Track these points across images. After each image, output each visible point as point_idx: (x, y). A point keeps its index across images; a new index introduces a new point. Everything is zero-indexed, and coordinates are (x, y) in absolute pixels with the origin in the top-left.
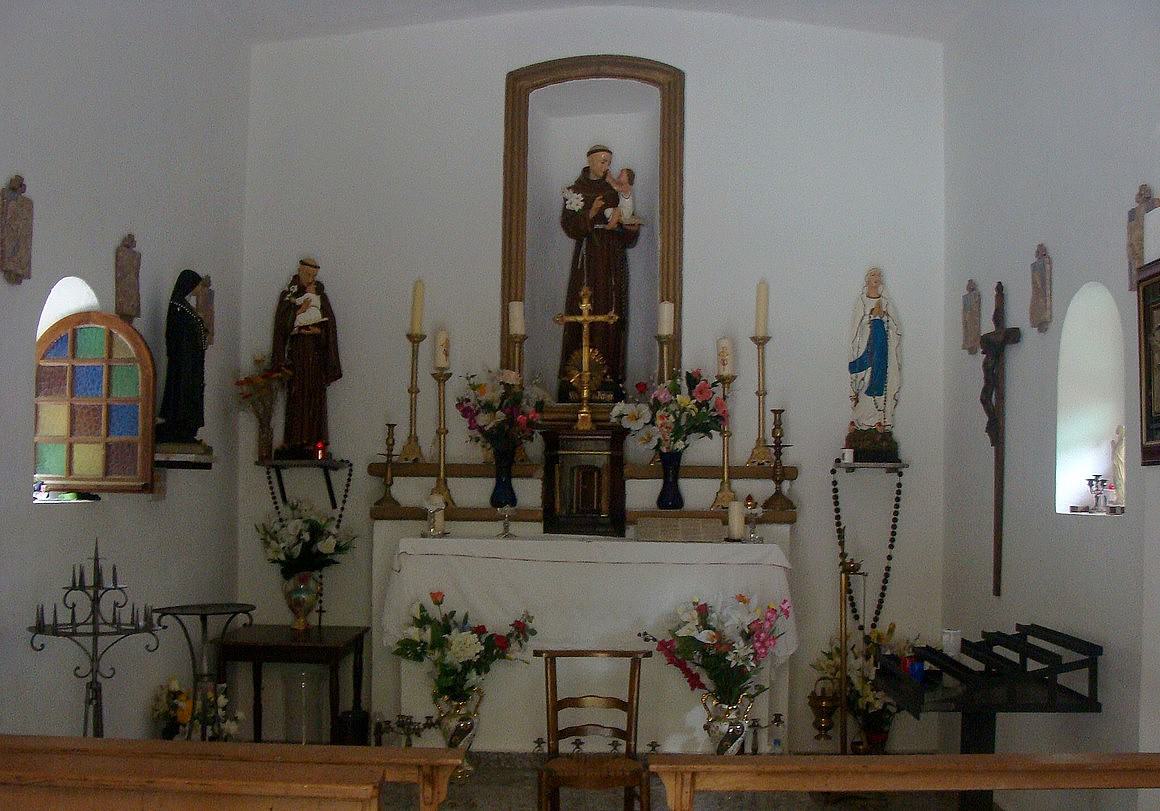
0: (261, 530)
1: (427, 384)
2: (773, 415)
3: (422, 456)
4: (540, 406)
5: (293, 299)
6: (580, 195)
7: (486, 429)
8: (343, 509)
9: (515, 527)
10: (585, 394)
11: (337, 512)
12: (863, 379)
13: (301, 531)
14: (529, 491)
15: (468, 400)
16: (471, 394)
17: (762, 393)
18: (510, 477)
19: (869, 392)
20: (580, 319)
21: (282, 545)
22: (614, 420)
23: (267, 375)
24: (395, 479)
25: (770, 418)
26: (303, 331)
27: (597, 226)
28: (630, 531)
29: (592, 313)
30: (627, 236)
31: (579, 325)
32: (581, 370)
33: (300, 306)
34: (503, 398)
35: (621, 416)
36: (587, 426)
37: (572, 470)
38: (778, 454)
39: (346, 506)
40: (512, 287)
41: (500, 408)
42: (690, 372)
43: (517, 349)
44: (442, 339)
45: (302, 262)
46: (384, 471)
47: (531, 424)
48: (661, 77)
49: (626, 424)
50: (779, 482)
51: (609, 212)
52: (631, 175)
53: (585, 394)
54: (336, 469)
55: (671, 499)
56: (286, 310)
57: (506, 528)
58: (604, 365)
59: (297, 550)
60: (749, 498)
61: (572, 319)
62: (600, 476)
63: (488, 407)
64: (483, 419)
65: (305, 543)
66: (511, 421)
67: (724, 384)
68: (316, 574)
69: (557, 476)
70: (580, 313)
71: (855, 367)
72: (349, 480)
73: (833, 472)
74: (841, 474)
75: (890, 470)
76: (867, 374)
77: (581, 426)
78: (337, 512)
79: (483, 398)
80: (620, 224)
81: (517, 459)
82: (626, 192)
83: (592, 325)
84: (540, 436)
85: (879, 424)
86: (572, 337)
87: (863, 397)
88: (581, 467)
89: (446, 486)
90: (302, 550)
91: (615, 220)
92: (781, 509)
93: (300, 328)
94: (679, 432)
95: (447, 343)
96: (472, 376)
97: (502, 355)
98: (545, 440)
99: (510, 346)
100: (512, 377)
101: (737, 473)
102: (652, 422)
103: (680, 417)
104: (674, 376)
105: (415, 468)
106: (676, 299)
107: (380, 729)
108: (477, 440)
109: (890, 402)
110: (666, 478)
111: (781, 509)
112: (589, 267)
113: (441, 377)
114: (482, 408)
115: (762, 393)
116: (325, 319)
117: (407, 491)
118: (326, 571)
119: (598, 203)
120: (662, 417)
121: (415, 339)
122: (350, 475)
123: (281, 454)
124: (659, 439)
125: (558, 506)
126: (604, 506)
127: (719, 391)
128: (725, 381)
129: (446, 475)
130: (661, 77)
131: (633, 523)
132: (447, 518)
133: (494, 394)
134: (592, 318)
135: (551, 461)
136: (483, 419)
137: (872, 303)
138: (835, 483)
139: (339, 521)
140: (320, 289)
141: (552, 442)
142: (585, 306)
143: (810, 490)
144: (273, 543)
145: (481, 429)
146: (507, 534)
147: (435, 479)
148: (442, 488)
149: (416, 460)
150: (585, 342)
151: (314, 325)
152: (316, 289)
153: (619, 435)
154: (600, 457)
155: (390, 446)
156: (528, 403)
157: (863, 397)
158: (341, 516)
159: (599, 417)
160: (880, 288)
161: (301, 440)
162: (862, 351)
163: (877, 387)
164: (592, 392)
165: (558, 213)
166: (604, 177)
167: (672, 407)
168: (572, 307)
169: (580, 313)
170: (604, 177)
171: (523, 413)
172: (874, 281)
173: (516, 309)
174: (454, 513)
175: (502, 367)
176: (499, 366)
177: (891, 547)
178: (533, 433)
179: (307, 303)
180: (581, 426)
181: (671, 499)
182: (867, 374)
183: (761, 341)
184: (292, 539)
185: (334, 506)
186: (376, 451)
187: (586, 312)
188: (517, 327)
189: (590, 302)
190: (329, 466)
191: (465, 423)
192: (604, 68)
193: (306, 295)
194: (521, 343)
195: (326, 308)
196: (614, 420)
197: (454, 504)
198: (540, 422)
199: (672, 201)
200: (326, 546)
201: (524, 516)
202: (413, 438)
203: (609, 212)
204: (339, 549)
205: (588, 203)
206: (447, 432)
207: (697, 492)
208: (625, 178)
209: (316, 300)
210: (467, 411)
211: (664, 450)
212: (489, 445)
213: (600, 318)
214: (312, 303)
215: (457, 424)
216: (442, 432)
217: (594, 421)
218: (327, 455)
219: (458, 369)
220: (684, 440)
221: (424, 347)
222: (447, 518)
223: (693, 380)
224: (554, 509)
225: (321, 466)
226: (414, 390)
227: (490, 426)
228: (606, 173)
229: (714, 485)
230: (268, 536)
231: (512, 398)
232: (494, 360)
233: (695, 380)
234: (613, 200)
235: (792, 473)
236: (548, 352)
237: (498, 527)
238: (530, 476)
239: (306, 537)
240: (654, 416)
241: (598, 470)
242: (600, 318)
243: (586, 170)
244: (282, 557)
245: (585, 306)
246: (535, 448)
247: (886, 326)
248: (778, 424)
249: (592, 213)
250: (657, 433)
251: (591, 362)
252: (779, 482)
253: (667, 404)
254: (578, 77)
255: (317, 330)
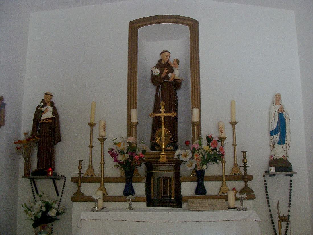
0: (24, 206)
1: (97, 144)
2: (243, 153)
3: (94, 174)
4: (144, 152)
5: (41, 109)
6: (158, 69)
7: (121, 161)
8: (61, 196)
9: (135, 205)
10: (163, 146)
11: (59, 197)
12: (276, 138)
13: (41, 206)
14: (140, 188)
15: (113, 150)
16: (115, 147)
17: (235, 145)
18: (131, 182)
19: (279, 143)
20: (160, 115)
21: (33, 213)
22: (176, 157)
23: (28, 140)
24: (83, 184)
25: (240, 155)
26: (44, 121)
27: (165, 81)
28: (184, 205)
29: (165, 112)
30: (177, 84)
31: (160, 118)
32: (160, 137)
33: (43, 112)
34: (128, 149)
35: (179, 155)
36: (165, 160)
37: (158, 179)
38: (245, 170)
39: (63, 195)
40: (132, 103)
41: (127, 152)
42: (208, 136)
43: (134, 128)
44: (102, 124)
45: (45, 94)
46: (78, 180)
47: (140, 159)
48: (189, 23)
49: (181, 158)
50: (246, 182)
51: (170, 75)
52: (178, 61)
53: (163, 146)
54: (59, 179)
55: (200, 191)
56: (39, 112)
57: (130, 205)
58: (170, 134)
59: (40, 215)
60: (234, 189)
61: (157, 115)
62: (170, 182)
63: (122, 152)
64: (120, 158)
65: (43, 212)
66: (132, 158)
67: (222, 141)
68: (50, 225)
69: (152, 182)
70: (160, 112)
71: (272, 133)
72: (64, 184)
73: (264, 176)
74: (268, 178)
75: (287, 175)
76: (278, 136)
77: (161, 160)
78: (59, 197)
79: (120, 148)
80: (174, 80)
81: (135, 175)
82: (176, 67)
83: (165, 117)
84: (144, 165)
85: (284, 156)
86: (157, 123)
87: (276, 145)
88: (162, 178)
89: (104, 187)
90: (42, 214)
91: (173, 78)
92: (250, 195)
93: (43, 120)
94: (205, 161)
95: (105, 125)
96: (115, 139)
97: (128, 132)
98: (146, 166)
99: (131, 127)
100: (132, 140)
101: (228, 178)
102: (193, 158)
103: (205, 155)
104: (200, 138)
105: (91, 179)
106: (199, 107)
107: (98, 190)
108: (117, 166)
109: (288, 147)
110: (198, 182)
111: (250, 195)
112: (162, 96)
113: (102, 139)
114: (119, 153)
115: (235, 145)
116: (54, 116)
117: (88, 189)
118: (54, 223)
119: (166, 71)
120: (197, 155)
121: (92, 125)
122: (65, 182)
123: (35, 173)
124: (196, 165)
125: (152, 194)
126: (173, 194)
127: (219, 144)
128: (221, 139)
129: (104, 182)
130: (189, 23)
131: (186, 201)
132: (104, 200)
133: (124, 147)
134: (165, 115)
135: (149, 176)
136: (120, 158)
137: (278, 107)
138: (265, 181)
139: (60, 201)
140: (52, 104)
141: (150, 167)
142: (162, 109)
143: (256, 185)
144: (29, 212)
145: (119, 162)
146: (131, 208)
147: (99, 184)
148: (102, 188)
149: (92, 175)
150: (163, 125)
151: (49, 119)
152: (51, 104)
153: (177, 163)
154: (170, 173)
155: (80, 169)
156: (139, 151)
157: (276, 145)
158: (61, 199)
159: (170, 156)
160: (280, 101)
161: (43, 168)
162: (275, 127)
163: (282, 141)
164: (166, 146)
165: (149, 77)
166: (168, 62)
167: (201, 151)
168: (157, 109)
169: (160, 112)
170: (168, 62)
171: (137, 155)
172: (278, 98)
173: (134, 112)
174: (107, 198)
175: (128, 136)
176: (126, 135)
177: (289, 207)
178: (141, 163)
179: (47, 110)
180: (161, 160)
181: (200, 191)
182: (278, 136)
183: (233, 124)
184: (38, 210)
185: (58, 195)
186: (74, 172)
187: (163, 112)
188: (134, 119)
189: (165, 107)
190: (55, 178)
191: (112, 159)
192: (167, 20)
193: (46, 107)
194: (136, 126)
195: (55, 112)
196: (176, 157)
197: (107, 194)
198: (144, 158)
199: (195, 69)
200: (52, 213)
201: (138, 199)
202: (91, 166)
203: (170, 75)
204: (58, 214)
205: (161, 72)
206: (105, 163)
207: (212, 188)
208: (176, 62)
209: (50, 109)
210: (113, 154)
211: (198, 169)
212: (122, 169)
213: (169, 114)
214: (49, 110)
215: (109, 160)
216: (103, 163)
217: (167, 158)
218: (54, 174)
219: (110, 135)
220: (206, 165)
221: (95, 128)
222: (104, 200)
223: (209, 139)
224: (151, 196)
225: (51, 178)
226: (91, 147)
227: (123, 160)
228: (168, 60)
229: (218, 184)
230: (28, 209)
231: (132, 148)
232: (124, 133)
233: (210, 139)
234: (171, 71)
235: (250, 178)
236: (146, 130)
237: (126, 205)
238: (140, 182)
239: (44, 209)
240: (193, 155)
241: (170, 179)
242: (169, 114)
243: (160, 61)
244: (33, 218)
245: (162, 109)
246: (142, 170)
247: (284, 116)
248: (245, 157)
249: (163, 75)
250: (195, 162)
251: (165, 133)
252: (246, 182)
253: (198, 150)
254: (157, 23)
255: (50, 121)
